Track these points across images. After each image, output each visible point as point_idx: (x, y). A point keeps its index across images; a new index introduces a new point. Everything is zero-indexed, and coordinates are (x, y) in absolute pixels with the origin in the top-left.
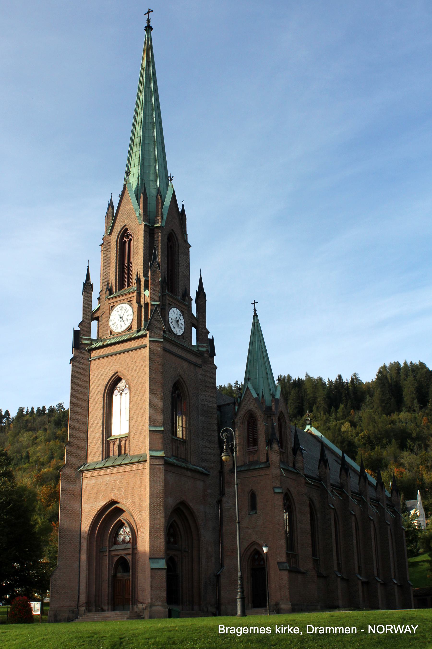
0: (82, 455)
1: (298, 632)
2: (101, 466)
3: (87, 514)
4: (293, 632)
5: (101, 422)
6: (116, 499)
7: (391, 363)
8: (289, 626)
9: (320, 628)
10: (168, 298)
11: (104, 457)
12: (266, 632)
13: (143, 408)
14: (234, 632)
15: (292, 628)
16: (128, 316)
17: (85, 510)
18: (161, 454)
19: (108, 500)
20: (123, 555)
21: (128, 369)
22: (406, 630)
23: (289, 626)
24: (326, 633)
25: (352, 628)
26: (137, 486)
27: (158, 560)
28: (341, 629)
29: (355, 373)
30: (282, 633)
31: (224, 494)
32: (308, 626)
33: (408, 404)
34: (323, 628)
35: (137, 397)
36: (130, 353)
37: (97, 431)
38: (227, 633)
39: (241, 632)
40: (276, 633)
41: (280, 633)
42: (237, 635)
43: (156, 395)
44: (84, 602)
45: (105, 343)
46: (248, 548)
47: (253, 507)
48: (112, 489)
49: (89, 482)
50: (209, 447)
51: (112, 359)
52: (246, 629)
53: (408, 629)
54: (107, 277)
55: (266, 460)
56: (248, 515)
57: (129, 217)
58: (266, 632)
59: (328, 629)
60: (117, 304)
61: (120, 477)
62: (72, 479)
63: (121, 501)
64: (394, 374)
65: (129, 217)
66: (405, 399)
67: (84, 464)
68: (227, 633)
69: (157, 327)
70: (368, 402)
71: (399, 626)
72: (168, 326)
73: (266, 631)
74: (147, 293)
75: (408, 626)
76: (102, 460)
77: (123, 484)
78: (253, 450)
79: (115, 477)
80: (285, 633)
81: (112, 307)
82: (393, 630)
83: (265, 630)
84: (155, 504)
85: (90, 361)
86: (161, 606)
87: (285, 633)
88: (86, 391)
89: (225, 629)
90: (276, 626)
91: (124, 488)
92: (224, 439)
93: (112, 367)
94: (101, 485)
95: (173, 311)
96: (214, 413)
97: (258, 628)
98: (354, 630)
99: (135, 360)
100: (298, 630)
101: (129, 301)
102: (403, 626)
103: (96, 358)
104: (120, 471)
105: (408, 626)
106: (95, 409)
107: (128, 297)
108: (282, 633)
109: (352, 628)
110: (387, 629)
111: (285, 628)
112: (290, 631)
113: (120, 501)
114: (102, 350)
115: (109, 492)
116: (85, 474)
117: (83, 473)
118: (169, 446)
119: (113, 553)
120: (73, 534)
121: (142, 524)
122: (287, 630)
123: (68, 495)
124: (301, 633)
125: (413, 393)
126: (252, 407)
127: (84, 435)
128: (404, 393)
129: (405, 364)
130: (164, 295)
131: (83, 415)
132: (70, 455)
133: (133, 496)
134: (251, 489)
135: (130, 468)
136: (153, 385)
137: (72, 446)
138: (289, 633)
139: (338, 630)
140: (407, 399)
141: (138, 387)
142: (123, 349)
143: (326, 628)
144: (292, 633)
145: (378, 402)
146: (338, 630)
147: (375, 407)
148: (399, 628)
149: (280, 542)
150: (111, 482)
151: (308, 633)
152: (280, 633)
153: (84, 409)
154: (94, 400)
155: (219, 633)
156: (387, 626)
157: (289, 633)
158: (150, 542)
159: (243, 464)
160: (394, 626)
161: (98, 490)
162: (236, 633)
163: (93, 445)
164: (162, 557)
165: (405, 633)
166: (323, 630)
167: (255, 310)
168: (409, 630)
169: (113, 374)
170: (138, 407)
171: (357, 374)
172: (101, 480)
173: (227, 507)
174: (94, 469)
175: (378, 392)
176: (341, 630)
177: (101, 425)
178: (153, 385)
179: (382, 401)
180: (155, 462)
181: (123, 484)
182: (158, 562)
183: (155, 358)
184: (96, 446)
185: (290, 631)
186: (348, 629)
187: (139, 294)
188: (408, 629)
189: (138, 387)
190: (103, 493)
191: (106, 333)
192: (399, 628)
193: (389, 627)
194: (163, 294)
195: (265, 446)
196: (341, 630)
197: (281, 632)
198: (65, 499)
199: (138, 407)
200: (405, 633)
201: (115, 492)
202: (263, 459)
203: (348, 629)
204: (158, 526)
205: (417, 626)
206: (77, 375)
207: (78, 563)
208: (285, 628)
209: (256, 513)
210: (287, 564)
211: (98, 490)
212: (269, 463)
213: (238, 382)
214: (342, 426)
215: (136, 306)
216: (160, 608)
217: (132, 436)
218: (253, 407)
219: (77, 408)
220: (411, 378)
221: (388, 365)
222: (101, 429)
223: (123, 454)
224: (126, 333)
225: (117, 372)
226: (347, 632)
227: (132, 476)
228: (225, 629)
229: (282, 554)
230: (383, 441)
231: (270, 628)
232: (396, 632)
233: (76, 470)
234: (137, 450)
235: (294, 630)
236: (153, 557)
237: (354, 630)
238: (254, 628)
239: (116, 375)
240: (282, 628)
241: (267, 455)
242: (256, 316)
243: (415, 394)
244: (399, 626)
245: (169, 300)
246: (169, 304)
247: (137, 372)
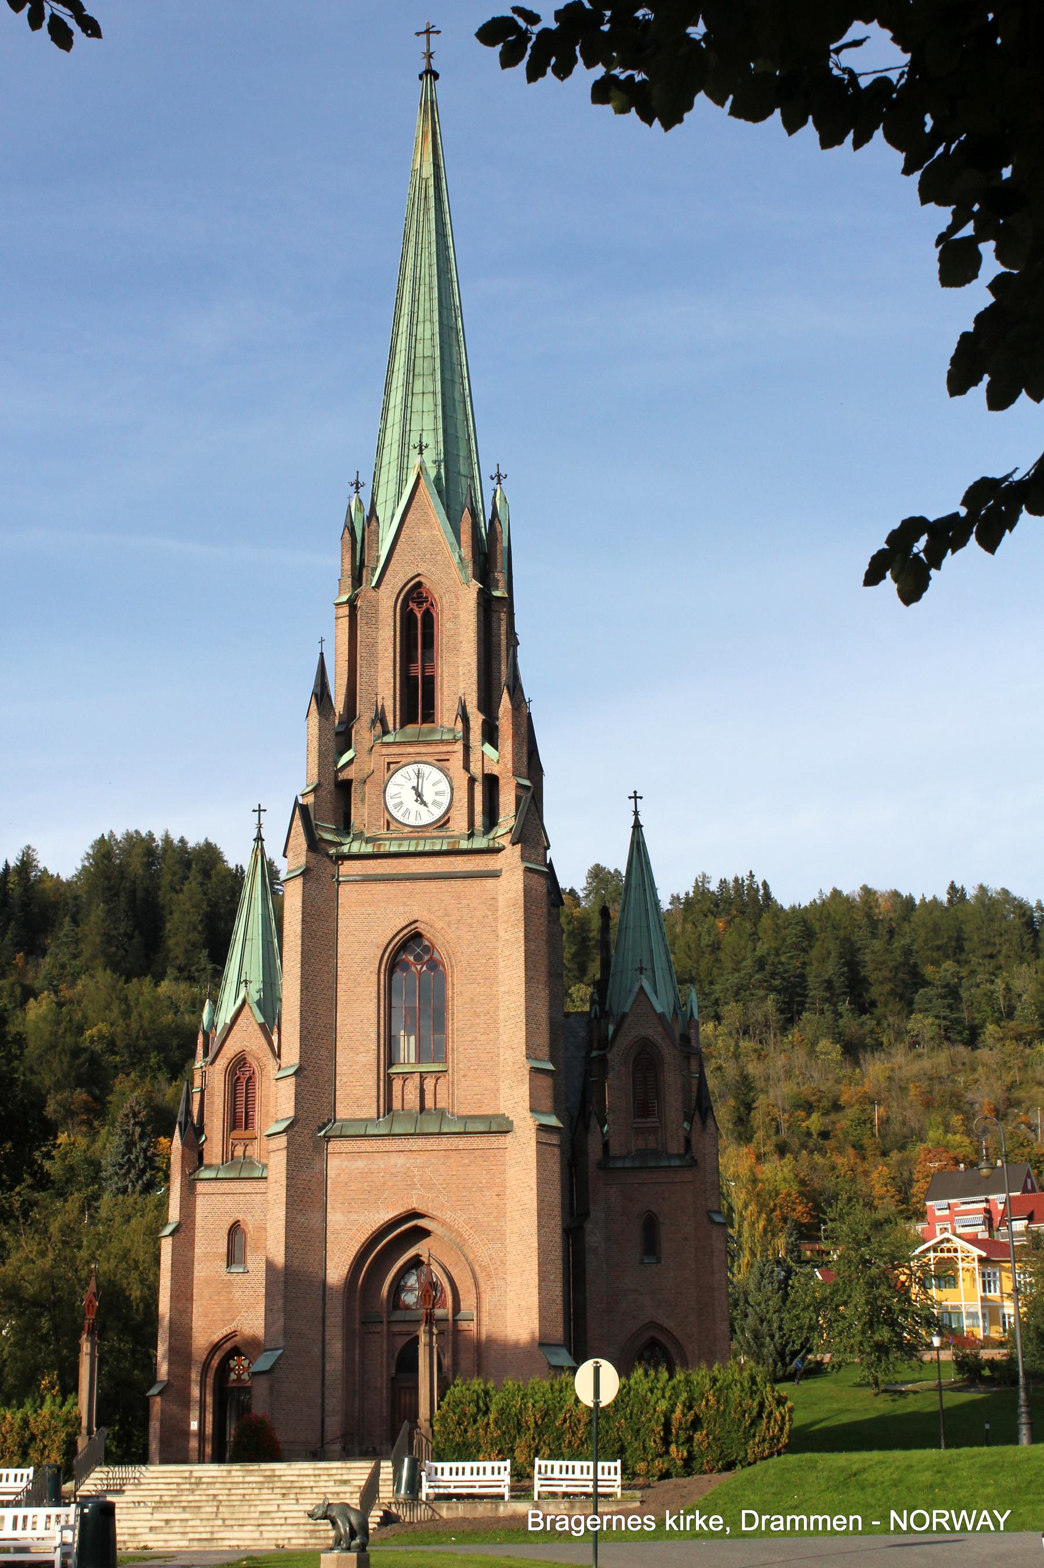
1: (721, 1527)
3: (341, 1236)
4: (708, 1526)
5: (373, 1029)
6: (421, 1208)
7: (127, 834)
8: (697, 1512)
9: (773, 1518)
11: (382, 1110)
12: (642, 1528)
13: (492, 1013)
14: (567, 1528)
15: (705, 1517)
17: (337, 1227)
18: (553, 1121)
19: (402, 1210)
21: (446, 918)
22: (981, 1523)
23: (697, 1512)
24: (788, 1528)
25: (851, 1518)
28: (824, 1521)
29: (29, 847)
30: (682, 1529)
32: (744, 1512)
33: (177, 957)
34: (781, 1517)
36: (453, 882)
37: (362, 1049)
38: (548, 1529)
39: (582, 1528)
40: (668, 1528)
41: (676, 1529)
42: (573, 1533)
47: (651, 1246)
48: (412, 1186)
49: (346, 1163)
51: (402, 887)
52: (595, 1520)
53: (985, 1520)
58: (642, 1528)
59: (793, 1521)
60: (404, 760)
61: (434, 1161)
63: (439, 1215)
64: (136, 866)
66: (171, 942)
67: (329, 1121)
68: (548, 1529)
70: (66, 936)
71: (964, 1513)
73: (643, 1523)
75: (985, 1513)
76: (378, 1118)
78: (645, 1125)
79: (420, 1160)
80: (688, 1529)
82: (950, 1522)
83: (639, 1522)
85: (339, 883)
87: (688, 1529)
88: (331, 952)
89: (544, 1519)
90: (668, 1512)
95: (439, 782)
97: (623, 1518)
98: (856, 1521)
100: (721, 1522)
102: (975, 1512)
103: (358, 878)
104: (435, 1148)
105: (985, 1513)
106: (355, 998)
108: (682, 1529)
109: (851, 1518)
110: (935, 1520)
111: (689, 1518)
112: (700, 1525)
113: (435, 1213)
114: (371, 863)
115: (405, 1192)
116: (333, 1146)
117: (328, 1142)
119: (396, 1328)
122: (693, 1522)
124: (728, 1529)
125: (195, 928)
128: (168, 925)
129: (167, 840)
135: (461, 1142)
137: (305, 1077)
138: (697, 1528)
139: (816, 1522)
140: (177, 944)
143: (789, 1518)
144: (706, 1528)
145: (98, 939)
146: (816, 1522)
147: (86, 954)
148: (964, 1519)
150: (409, 1168)
151: (744, 1528)
152: (676, 1529)
154: (352, 977)
155: (530, 1528)
156: (935, 1512)
157: (697, 1528)
158: (540, 1311)
160: (953, 1512)
162: (571, 1529)
164: (559, 1342)
165: (978, 1528)
166: (781, 1522)
167: (636, 813)
168: (989, 1522)
169: (404, 924)
171: (34, 850)
172: (380, 1163)
175: (99, 912)
176: (825, 1521)
177: (374, 1036)
179: (108, 939)
180: (547, 1138)
185: (700, 1525)
186: (840, 1520)
187: (467, 748)
188: (985, 1520)
192: (964, 1519)
193: (939, 1516)
196: (825, 1521)
197: (678, 1526)
200: (978, 1528)
201: (423, 1192)
202: (675, 1146)
203: (840, 1520)
204: (552, 1277)
205: (1008, 1512)
207: (320, 1346)
208: (689, 1518)
209: (659, 1261)
214: (32, 1000)
215: (461, 780)
217: (462, 1073)
218: (653, 1032)
220: (192, 885)
221: (119, 837)
222: (374, 1047)
223: (430, 1109)
225: (416, 921)
226: (839, 1526)
227: (467, 1161)
228: (544, 1519)
230: (149, 1058)
231: (653, 1518)
232: (958, 1527)
233: (314, 1135)
235: (711, 1522)
236: (545, 1341)
237: (856, 1521)
238: (615, 1518)
239: (413, 927)
240: (682, 1517)
241: (688, 1142)
242: (637, 826)
243: (199, 933)
244: (964, 1513)
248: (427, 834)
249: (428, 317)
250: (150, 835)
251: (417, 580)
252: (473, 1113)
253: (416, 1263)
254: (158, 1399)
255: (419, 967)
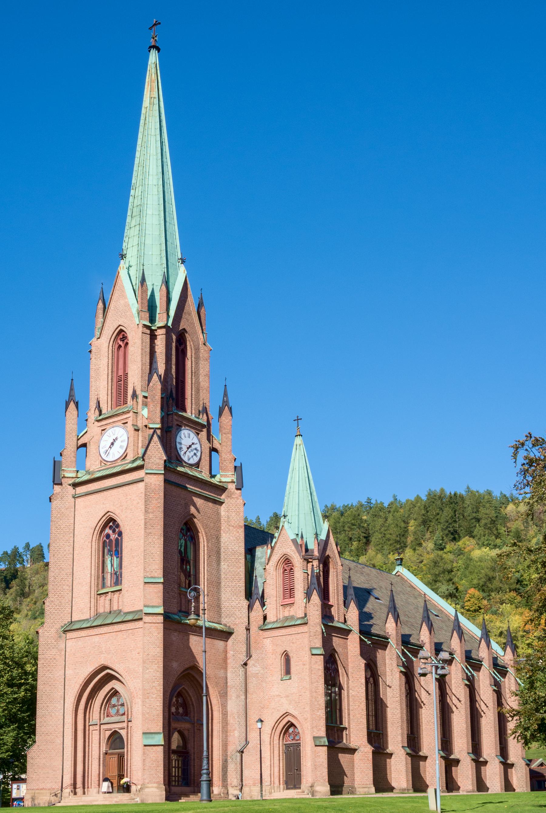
0: (65, 612)
2: (88, 625)
10: (175, 417)
16: (122, 442)
19: (97, 666)
20: (117, 729)
26: (131, 649)
27: (153, 735)
31: (251, 657)
35: (132, 541)
43: (154, 539)
44: (69, 783)
45: (93, 477)
46: (280, 720)
50: (233, 599)
51: (102, 495)
54: (96, 392)
55: (303, 616)
56: (280, 681)
57: (123, 314)
60: (108, 427)
62: (53, 640)
65: (123, 314)
69: (155, 457)
72: (176, 453)
74: (145, 412)
77: (114, 647)
81: (103, 430)
84: (151, 670)
86: (156, 787)
91: (115, 651)
92: (192, 599)
93: (102, 506)
94: (89, 648)
95: (184, 434)
96: (240, 558)
99: (130, 497)
101: (124, 423)
107: (122, 418)
115: (99, 656)
118: (175, 600)
120: (55, 705)
121: (137, 693)
123: (48, 660)
126: (288, 550)
127: (67, 588)
130: (170, 414)
131: (67, 565)
132: (51, 613)
133: (127, 661)
134: (284, 650)
136: (150, 527)
141: (134, 530)
142: (115, 484)
149: (319, 713)
153: (68, 556)
159: (275, 620)
161: (84, 653)
163: (79, 600)
169: (103, 515)
170: (134, 554)
173: (254, 672)
174: (100, 625)
178: (150, 527)
181: (114, 647)
182: (152, 738)
183: (153, 494)
184: (83, 601)
189: (134, 530)
190: (91, 657)
191: (96, 463)
194: (169, 413)
195: (303, 598)
198: (45, 664)
199: (134, 554)
204: (154, 696)
206: (59, 516)
210: (326, 739)
211: (84, 653)
212: (307, 619)
213: (370, 500)
216: (154, 790)
219: (59, 556)
224: (120, 464)
229: (320, 727)
234: (133, 606)
245: (176, 420)
246: (177, 425)
247: (133, 511)
248: (117, 464)
249: (141, 184)
250: (435, 490)
251: (119, 328)
252: (129, 611)
253: (115, 693)
254: (205, 775)
255: (114, 536)
